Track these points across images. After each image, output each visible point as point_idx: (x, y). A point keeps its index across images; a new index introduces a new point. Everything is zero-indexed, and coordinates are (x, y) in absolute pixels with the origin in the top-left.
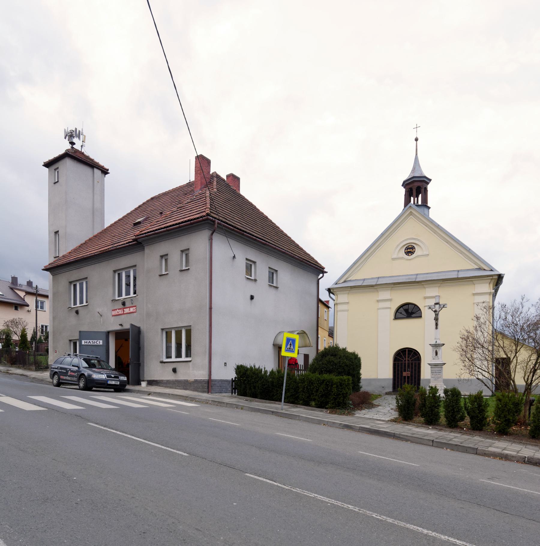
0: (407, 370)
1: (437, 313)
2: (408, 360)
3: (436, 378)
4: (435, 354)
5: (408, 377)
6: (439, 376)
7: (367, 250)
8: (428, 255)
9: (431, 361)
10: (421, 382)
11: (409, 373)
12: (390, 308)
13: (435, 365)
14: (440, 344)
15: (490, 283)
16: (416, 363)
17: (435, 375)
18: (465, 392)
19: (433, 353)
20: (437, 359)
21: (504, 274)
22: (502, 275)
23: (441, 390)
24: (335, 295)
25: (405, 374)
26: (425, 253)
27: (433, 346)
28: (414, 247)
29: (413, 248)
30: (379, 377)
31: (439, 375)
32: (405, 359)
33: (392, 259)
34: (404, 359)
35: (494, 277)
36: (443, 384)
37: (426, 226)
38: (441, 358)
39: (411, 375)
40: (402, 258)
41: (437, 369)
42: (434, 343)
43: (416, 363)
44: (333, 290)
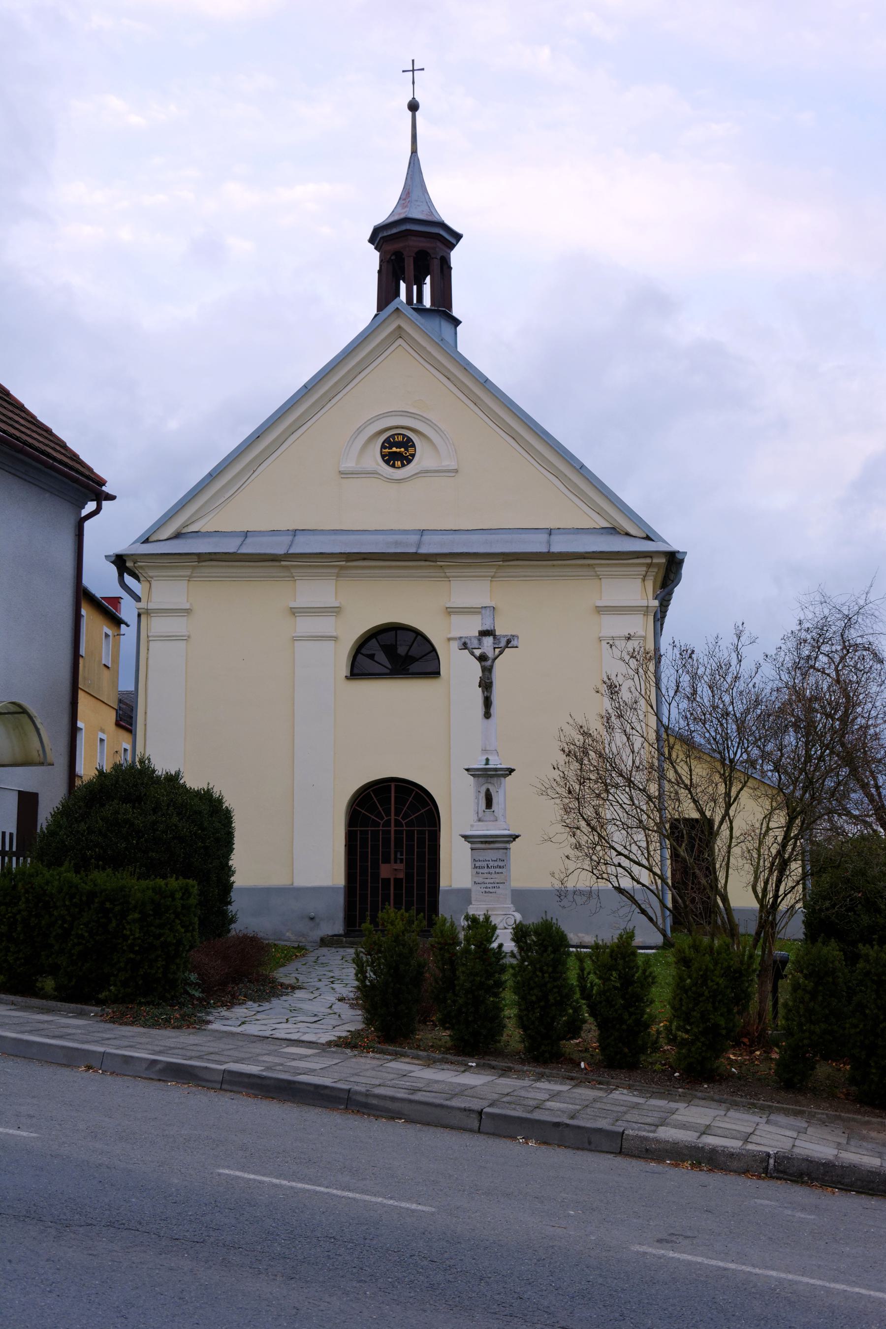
1: (489, 663)
2: (398, 823)
9: (472, 826)
12: (335, 638)
13: (486, 842)
15: (645, 576)
17: (485, 875)
18: (580, 935)
20: (493, 821)
22: (679, 556)
24: (142, 579)
25: (386, 871)
26: (449, 463)
29: (408, 443)
31: (496, 876)
34: (382, 819)
35: (655, 561)
38: (504, 816)
40: (373, 474)
41: (490, 855)
42: (481, 765)
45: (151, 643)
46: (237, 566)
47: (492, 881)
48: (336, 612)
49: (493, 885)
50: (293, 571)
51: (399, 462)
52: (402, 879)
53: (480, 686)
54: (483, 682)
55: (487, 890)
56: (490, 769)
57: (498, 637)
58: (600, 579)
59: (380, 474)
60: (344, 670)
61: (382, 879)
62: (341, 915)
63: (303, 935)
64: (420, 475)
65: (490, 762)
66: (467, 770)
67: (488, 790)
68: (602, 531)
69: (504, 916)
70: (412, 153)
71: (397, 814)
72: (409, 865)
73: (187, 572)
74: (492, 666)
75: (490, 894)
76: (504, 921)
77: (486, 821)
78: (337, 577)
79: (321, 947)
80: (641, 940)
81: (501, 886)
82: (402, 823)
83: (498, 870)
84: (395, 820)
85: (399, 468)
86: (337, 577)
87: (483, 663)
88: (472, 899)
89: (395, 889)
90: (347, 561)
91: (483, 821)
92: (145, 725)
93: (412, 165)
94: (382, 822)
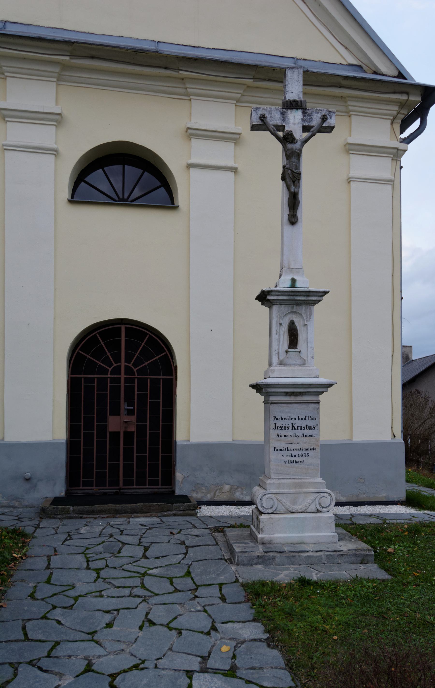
2: (128, 371)
3: (293, 453)
5: (126, 433)
6: (307, 443)
10: (179, 454)
11: (133, 419)
12: (55, 152)
17: (290, 439)
20: (300, 365)
23: (318, 511)
31: (305, 439)
34: (110, 365)
35: (412, 98)
36: (321, 480)
39: (138, 427)
47: (298, 446)
49: (300, 452)
52: (134, 432)
53: (283, 178)
55: (292, 459)
56: (300, 293)
57: (309, 112)
58: (350, 116)
60: (66, 194)
61: (110, 432)
62: (62, 474)
63: (16, 499)
65: (298, 284)
68: (350, 68)
69: (316, 495)
71: (128, 360)
72: (141, 418)
74: (301, 150)
76: (317, 501)
77: (290, 365)
80: (384, 495)
81: (311, 453)
83: (307, 432)
87: (289, 146)
90: (72, 56)
91: (285, 365)
94: (110, 369)
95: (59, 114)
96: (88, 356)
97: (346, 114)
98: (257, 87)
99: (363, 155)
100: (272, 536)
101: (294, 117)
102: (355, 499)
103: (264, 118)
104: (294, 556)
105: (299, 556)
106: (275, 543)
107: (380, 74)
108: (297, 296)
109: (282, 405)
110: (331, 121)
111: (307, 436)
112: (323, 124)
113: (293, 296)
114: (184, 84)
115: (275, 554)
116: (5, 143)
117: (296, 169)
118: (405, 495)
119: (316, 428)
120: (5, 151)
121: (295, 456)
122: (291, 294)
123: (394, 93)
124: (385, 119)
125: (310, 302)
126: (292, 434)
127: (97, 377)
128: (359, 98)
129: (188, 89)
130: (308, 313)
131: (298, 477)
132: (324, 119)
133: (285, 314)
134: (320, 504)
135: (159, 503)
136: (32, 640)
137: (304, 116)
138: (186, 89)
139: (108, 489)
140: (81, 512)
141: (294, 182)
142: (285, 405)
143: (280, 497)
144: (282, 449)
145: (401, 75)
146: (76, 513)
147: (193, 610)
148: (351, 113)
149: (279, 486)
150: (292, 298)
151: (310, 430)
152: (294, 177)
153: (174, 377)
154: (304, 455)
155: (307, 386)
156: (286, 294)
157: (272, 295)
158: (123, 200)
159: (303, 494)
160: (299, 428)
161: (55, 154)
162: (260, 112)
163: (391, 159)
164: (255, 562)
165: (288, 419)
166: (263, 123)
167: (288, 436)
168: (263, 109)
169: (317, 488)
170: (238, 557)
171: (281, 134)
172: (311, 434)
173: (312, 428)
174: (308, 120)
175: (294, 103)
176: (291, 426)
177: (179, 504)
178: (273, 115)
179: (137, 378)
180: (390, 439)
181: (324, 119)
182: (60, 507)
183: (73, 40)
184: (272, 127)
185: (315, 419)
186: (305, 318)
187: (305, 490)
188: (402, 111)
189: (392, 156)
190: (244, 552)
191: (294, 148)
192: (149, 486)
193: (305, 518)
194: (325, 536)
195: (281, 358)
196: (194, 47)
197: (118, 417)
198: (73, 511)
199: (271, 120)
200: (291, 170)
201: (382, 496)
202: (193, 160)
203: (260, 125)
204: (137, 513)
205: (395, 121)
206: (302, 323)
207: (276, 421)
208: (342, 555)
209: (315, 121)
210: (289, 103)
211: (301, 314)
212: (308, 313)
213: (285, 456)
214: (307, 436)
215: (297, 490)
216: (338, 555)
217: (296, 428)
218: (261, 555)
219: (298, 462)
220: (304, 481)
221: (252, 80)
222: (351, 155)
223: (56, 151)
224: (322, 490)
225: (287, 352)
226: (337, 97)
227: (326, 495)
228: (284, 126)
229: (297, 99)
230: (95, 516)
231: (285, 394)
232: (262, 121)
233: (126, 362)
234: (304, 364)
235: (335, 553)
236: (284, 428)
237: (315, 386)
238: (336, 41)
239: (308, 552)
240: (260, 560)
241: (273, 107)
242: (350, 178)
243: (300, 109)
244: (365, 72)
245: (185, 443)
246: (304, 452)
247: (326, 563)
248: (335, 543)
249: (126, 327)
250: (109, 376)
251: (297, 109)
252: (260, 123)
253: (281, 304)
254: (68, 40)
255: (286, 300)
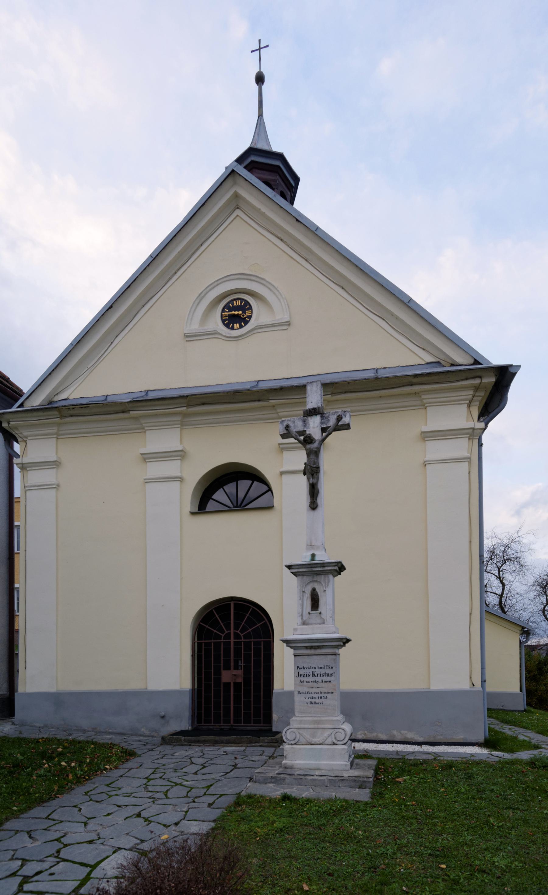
0: (232, 664)
1: (315, 445)
2: (237, 636)
3: (314, 696)
4: (308, 604)
5: (235, 684)
6: (325, 687)
7: (110, 307)
8: (288, 324)
9: (295, 630)
12: (180, 479)
13: (311, 648)
14: (329, 564)
15: (470, 402)
16: (259, 643)
18: (403, 732)
19: (301, 599)
20: (320, 624)
21: (519, 367)
22: (511, 370)
23: (334, 744)
24: (19, 439)
25: (227, 676)
26: (281, 316)
27: (302, 574)
28: (247, 303)
29: (246, 306)
30: (152, 687)
31: (324, 685)
32: (226, 632)
33: (186, 336)
34: (223, 632)
35: (485, 380)
37: (281, 240)
38: (333, 617)
40: (214, 334)
41: (316, 661)
42: (305, 559)
43: (259, 643)
44: (9, 424)
45: (28, 493)
46: (95, 421)
47: (318, 690)
48: (180, 456)
49: (320, 695)
50: (142, 421)
51: (238, 324)
54: (309, 467)
55: (313, 701)
58: (426, 408)
59: (221, 335)
64: (256, 331)
66: (289, 567)
67: (314, 590)
69: (332, 730)
70: (259, 117)
71: (236, 628)
73: (54, 430)
75: (317, 705)
76: (333, 735)
77: (311, 624)
78: (182, 425)
79: (161, 744)
80: (462, 737)
81: (329, 696)
82: (227, 634)
83: (325, 678)
84: (235, 633)
85: (237, 329)
86: (182, 425)
87: (308, 446)
88: (296, 710)
89: (235, 692)
90: (188, 406)
91: (307, 624)
92: (26, 560)
93: (258, 125)
94: (223, 635)
95: (182, 451)
96: (207, 627)
97: (422, 407)
98: (337, 400)
99: (439, 439)
100: (293, 762)
101: (314, 422)
102: (432, 740)
103: (288, 427)
104: (302, 778)
105: (306, 779)
106: (295, 768)
107: (457, 365)
108: (314, 567)
109: (304, 657)
110: (346, 420)
111: (325, 682)
112: (338, 423)
113: (311, 568)
114: (276, 410)
115: (286, 776)
116: (145, 478)
117: (314, 464)
118: (484, 738)
119: (333, 675)
120: (146, 484)
121: (315, 698)
122: (308, 566)
123: (467, 379)
124: (461, 404)
125: (327, 571)
126: (312, 680)
127: (204, 642)
128: (433, 391)
129: (279, 413)
130: (327, 581)
131: (318, 716)
132: (339, 418)
133: (307, 583)
134: (335, 738)
135: (248, 737)
136: (82, 822)
137: (322, 420)
138: (278, 413)
139: (226, 727)
140: (190, 741)
141: (313, 475)
142: (307, 657)
143: (301, 731)
144: (305, 692)
145: (476, 362)
146: (186, 742)
147: (178, 810)
148: (426, 405)
149: (301, 722)
150: (310, 569)
151: (328, 677)
152: (313, 471)
153: (272, 640)
154: (323, 698)
155: (321, 641)
156: (304, 566)
157: (293, 569)
158: (237, 506)
159: (321, 730)
160: (319, 675)
161: (180, 481)
162: (285, 424)
163: (467, 438)
164: (269, 781)
165: (309, 668)
166: (288, 432)
167: (309, 682)
168: (288, 420)
169: (333, 725)
170: (256, 776)
171: (302, 438)
172: (329, 680)
173: (330, 675)
174: (326, 423)
175: (313, 410)
176: (312, 674)
177: (264, 738)
178: (296, 424)
179: (223, 642)
180: (469, 688)
181: (339, 418)
182: (174, 737)
183: (186, 395)
184: (294, 434)
185: (332, 668)
186: (324, 585)
187: (323, 726)
188: (477, 394)
189: (469, 436)
190: (261, 773)
191: (312, 448)
192: (253, 723)
193: (321, 749)
194: (338, 764)
195: (304, 619)
196: (288, 378)
197: (230, 671)
198: (184, 740)
199: (295, 428)
200: (309, 466)
201: (460, 737)
202: (285, 469)
203: (286, 433)
204: (232, 743)
205: (472, 404)
206: (322, 590)
207: (299, 670)
208: (343, 780)
209: (332, 422)
210: (308, 411)
211: (320, 582)
212: (327, 581)
213: (307, 698)
214: (325, 682)
215: (316, 726)
216: (339, 780)
217: (316, 675)
218: (274, 776)
219: (318, 703)
220: (322, 718)
221: (330, 396)
222: (427, 442)
223: (180, 478)
224: (337, 727)
225: (309, 613)
226: (411, 394)
227: (340, 730)
228: (305, 431)
229: (315, 406)
230: (200, 744)
231: (305, 648)
232: (287, 430)
233: (235, 629)
234: (324, 623)
235: (336, 778)
236: (305, 675)
237: (328, 640)
238: (415, 346)
239: (313, 775)
240: (273, 780)
241: (296, 418)
242: (425, 462)
243: (318, 414)
244: (444, 366)
245: (280, 691)
246: (323, 695)
247: (328, 785)
248: (347, 770)
249: (234, 603)
250: (222, 640)
251: (316, 415)
252: (286, 432)
253: (303, 575)
254: (182, 395)
255: (305, 572)
